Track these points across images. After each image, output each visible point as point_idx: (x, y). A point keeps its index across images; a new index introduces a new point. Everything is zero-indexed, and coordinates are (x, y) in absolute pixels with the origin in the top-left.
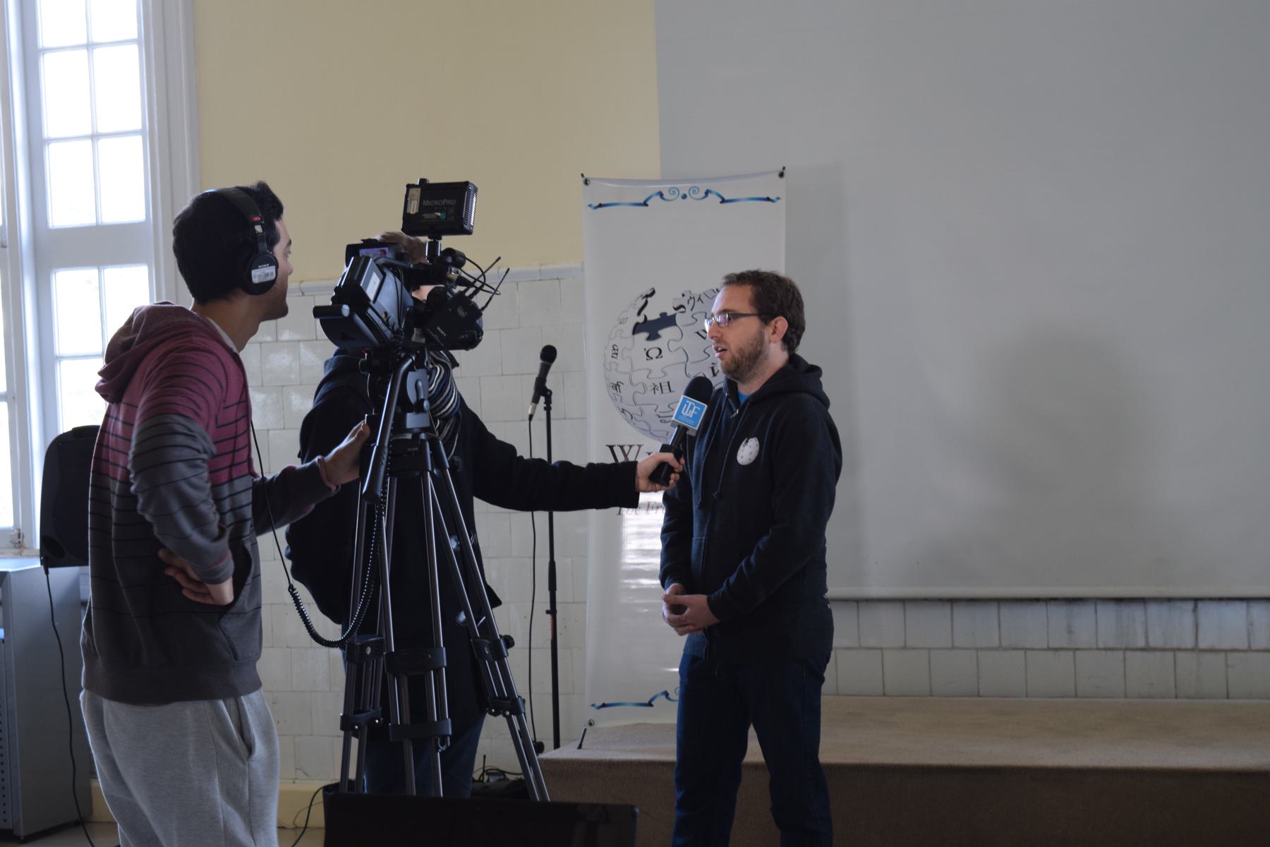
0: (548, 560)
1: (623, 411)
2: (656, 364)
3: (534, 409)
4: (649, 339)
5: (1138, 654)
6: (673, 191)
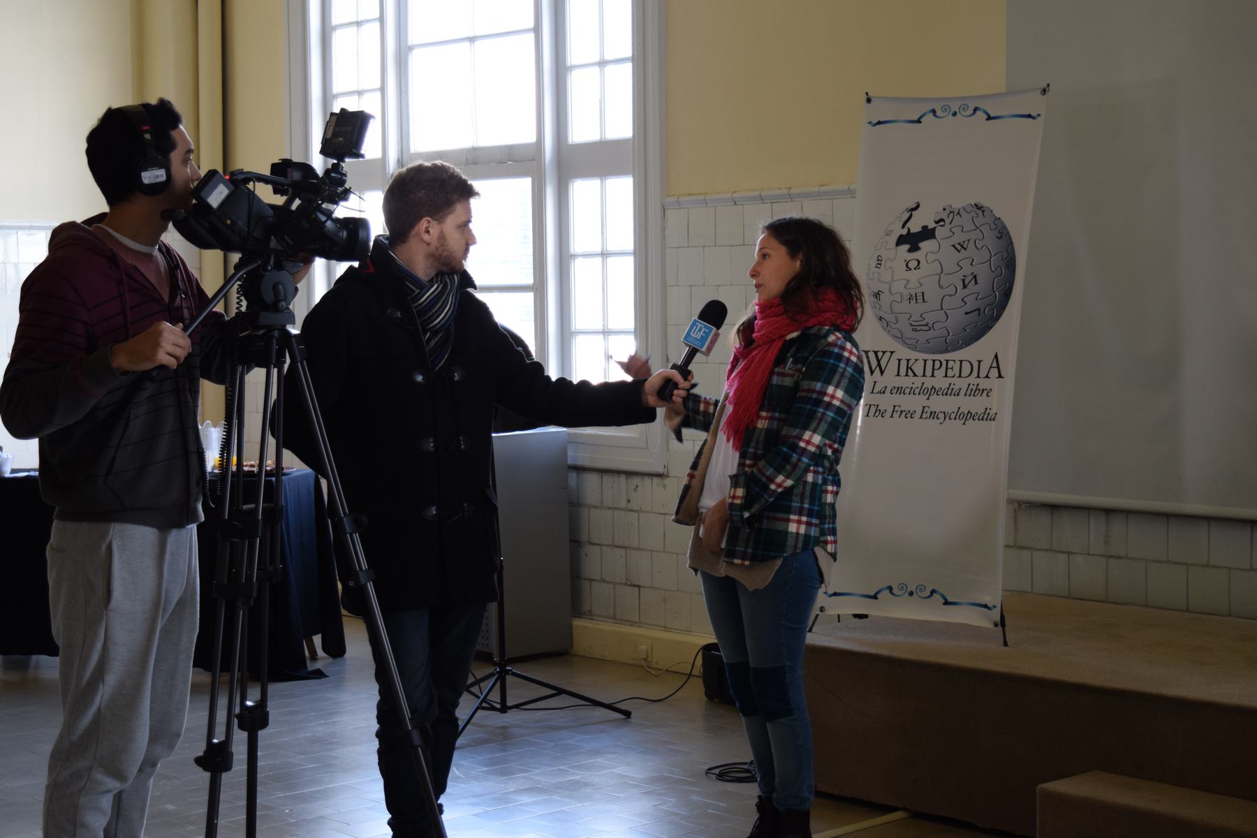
1: (881, 319)
2: (914, 276)
4: (910, 251)
6: (945, 108)
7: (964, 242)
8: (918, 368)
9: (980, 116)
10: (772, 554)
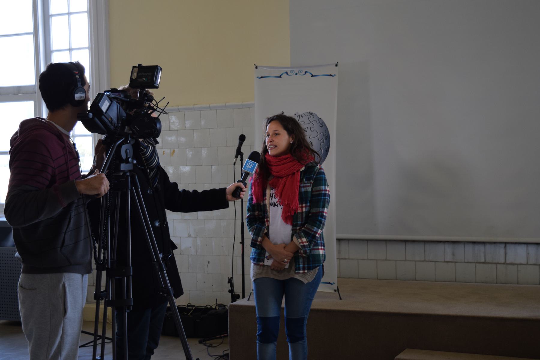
0: (241, 222)
3: (236, 160)
5: (482, 265)
6: (292, 72)
7: (305, 128)
10: (317, 265)
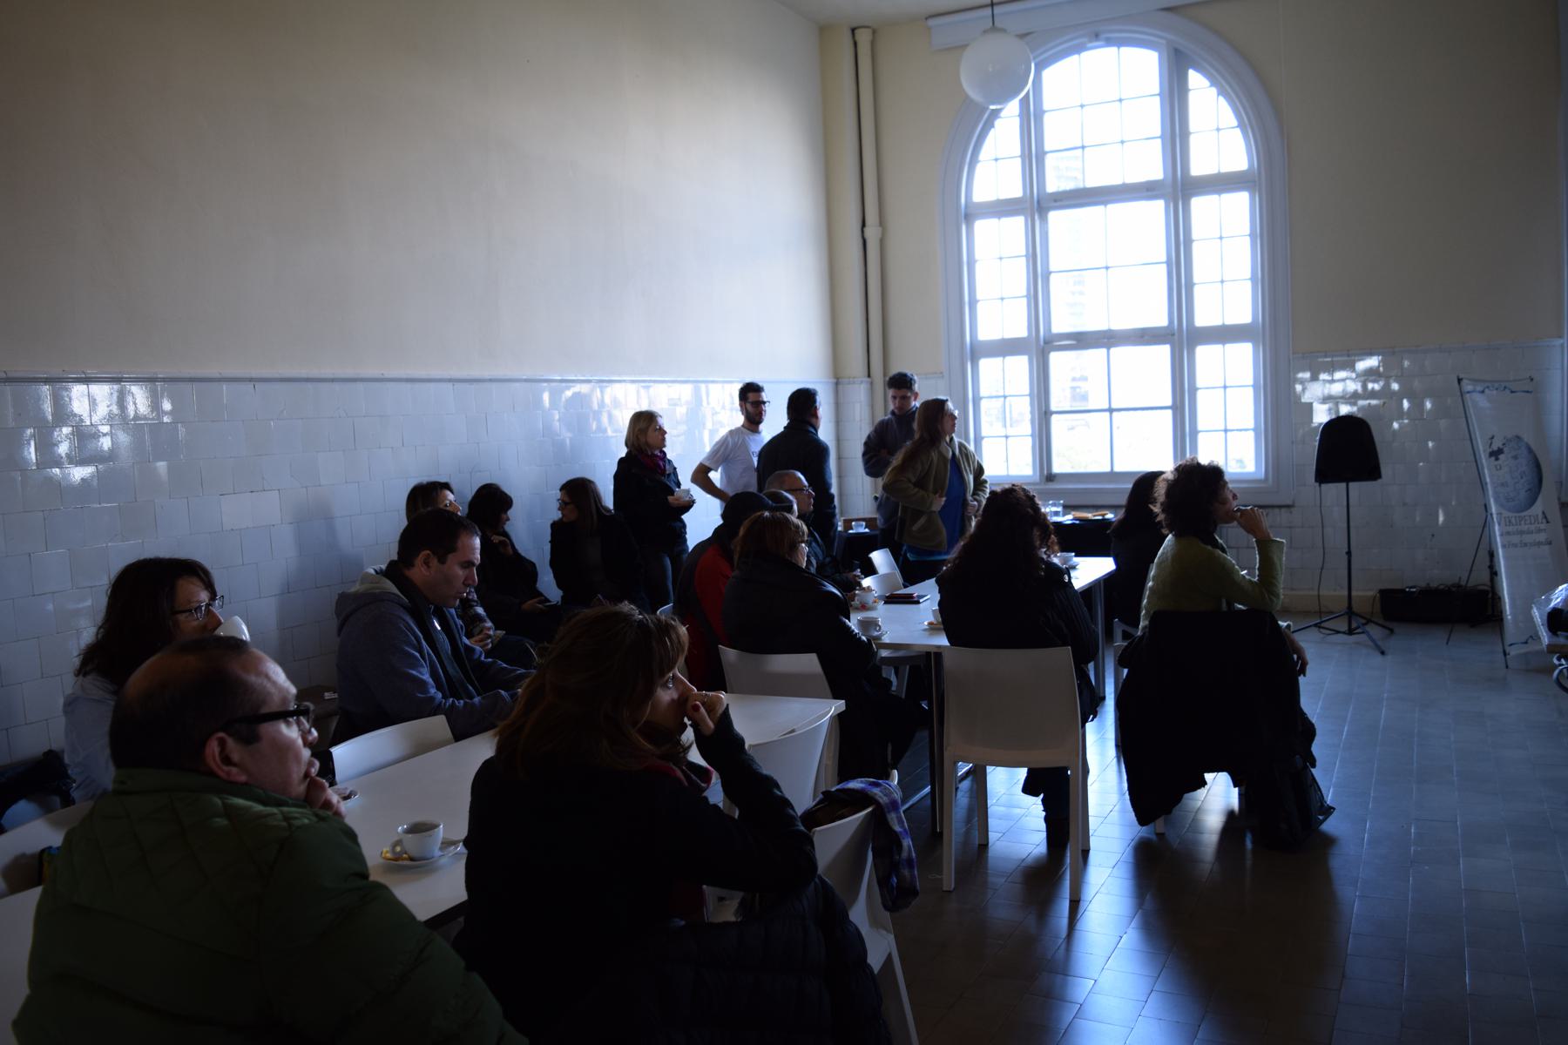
8: (1513, 520)
9: (1508, 391)
